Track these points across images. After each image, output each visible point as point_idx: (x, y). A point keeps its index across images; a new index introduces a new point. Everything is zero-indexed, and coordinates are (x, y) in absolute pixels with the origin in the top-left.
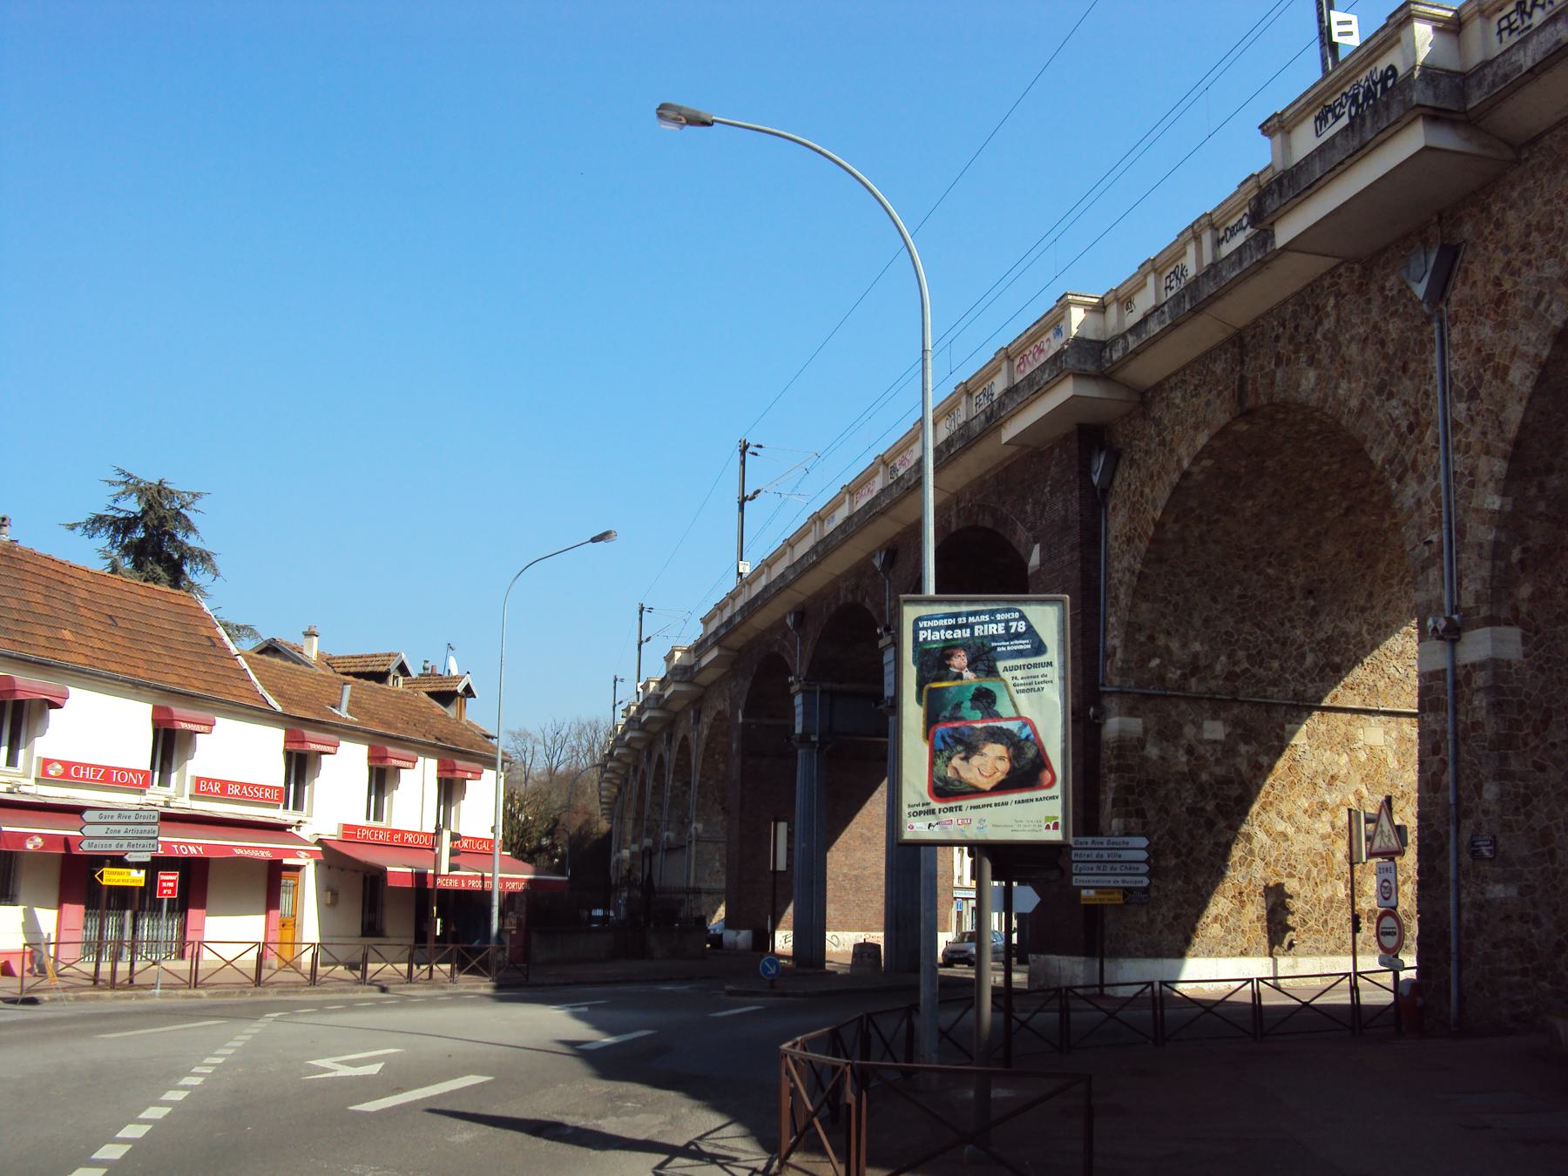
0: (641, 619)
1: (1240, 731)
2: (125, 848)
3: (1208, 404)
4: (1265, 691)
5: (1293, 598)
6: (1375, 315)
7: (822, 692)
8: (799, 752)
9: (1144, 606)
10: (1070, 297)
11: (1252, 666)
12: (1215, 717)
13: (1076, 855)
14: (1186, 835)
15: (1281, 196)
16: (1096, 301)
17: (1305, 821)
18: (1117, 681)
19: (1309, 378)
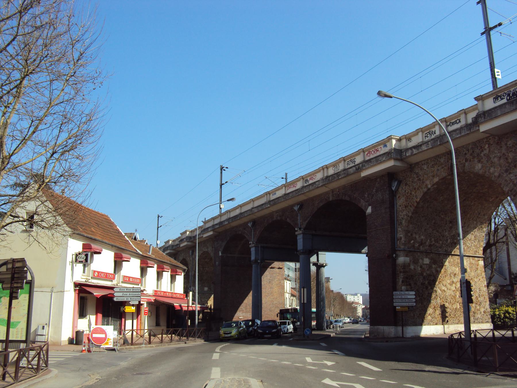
0: (158, 220)
1: (432, 261)
2: (129, 300)
3: (438, 170)
6: (504, 151)
7: (261, 247)
8: (253, 265)
9: (411, 226)
10: (392, 137)
11: (435, 243)
12: (426, 257)
13: (395, 297)
15: (484, 118)
16: (399, 138)
17: (449, 286)
18: (402, 247)
19: (478, 166)
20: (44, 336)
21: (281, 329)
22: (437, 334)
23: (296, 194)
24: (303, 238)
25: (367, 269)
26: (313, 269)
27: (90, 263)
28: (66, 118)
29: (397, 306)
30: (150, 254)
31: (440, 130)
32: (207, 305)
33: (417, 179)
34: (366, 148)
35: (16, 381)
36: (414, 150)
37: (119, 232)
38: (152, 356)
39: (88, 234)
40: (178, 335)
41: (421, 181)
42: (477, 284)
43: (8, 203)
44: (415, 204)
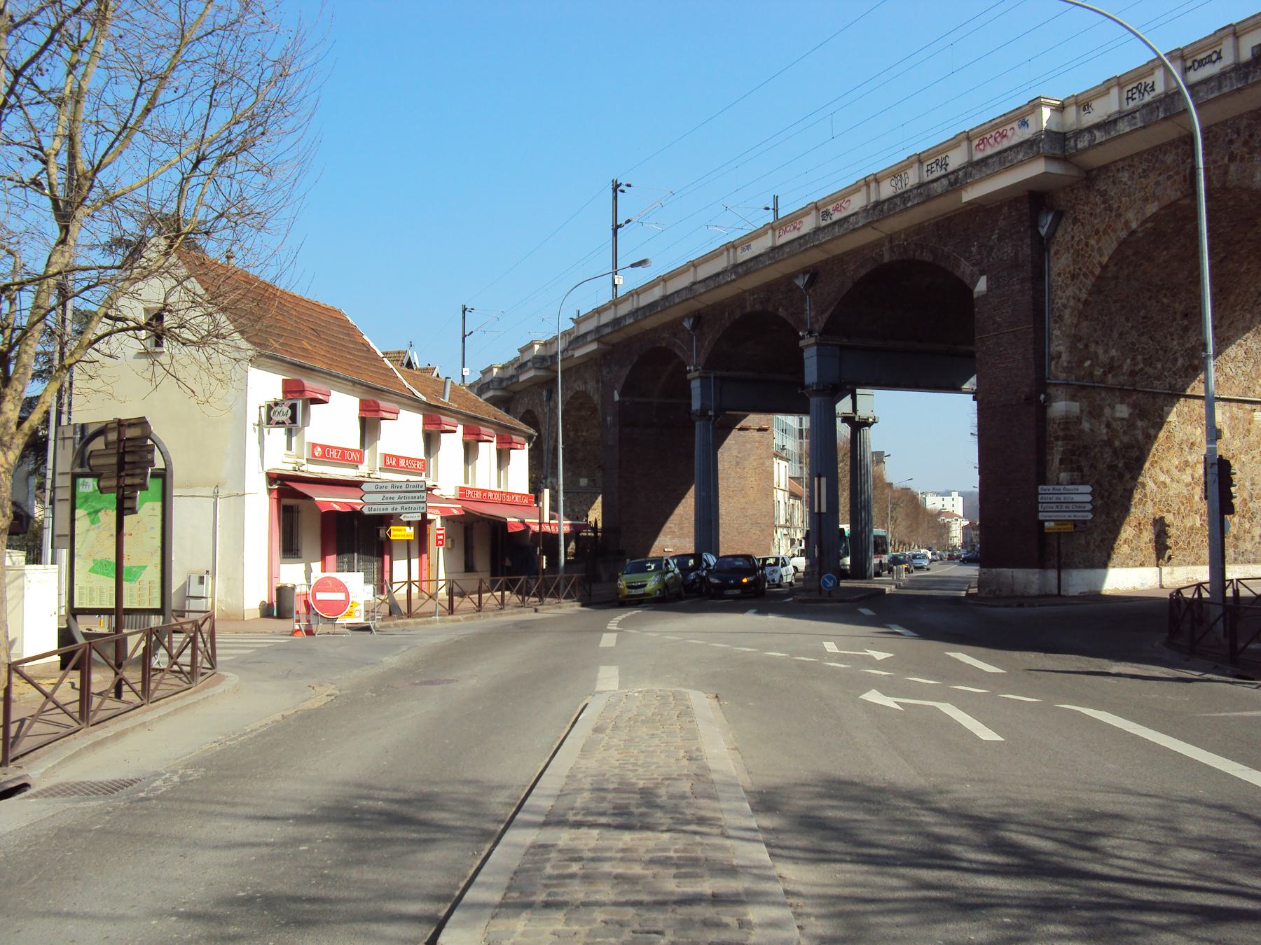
0: (464, 318)
1: (1137, 411)
2: (399, 511)
3: (1157, 183)
4: (1152, 384)
5: (1175, 319)
8: (697, 423)
9: (1085, 324)
10: (1042, 100)
11: (1146, 366)
14: (1107, 483)
16: (1058, 103)
17: (1176, 473)
18: (1063, 376)
20: (204, 600)
21: (764, 576)
22: (1142, 588)
23: (801, 246)
24: (819, 355)
25: (975, 431)
26: (843, 430)
27: (303, 426)
28: (223, 71)
29: (1047, 521)
30: (447, 400)
31: (1167, 82)
32: (587, 521)
33: (1103, 206)
34: (975, 131)
35: (145, 701)
36: (1097, 134)
37: (369, 350)
38: (457, 641)
39: (295, 355)
40: (519, 592)
41: (1114, 213)
42: (1247, 469)
43: (96, 285)
44: (1097, 271)
